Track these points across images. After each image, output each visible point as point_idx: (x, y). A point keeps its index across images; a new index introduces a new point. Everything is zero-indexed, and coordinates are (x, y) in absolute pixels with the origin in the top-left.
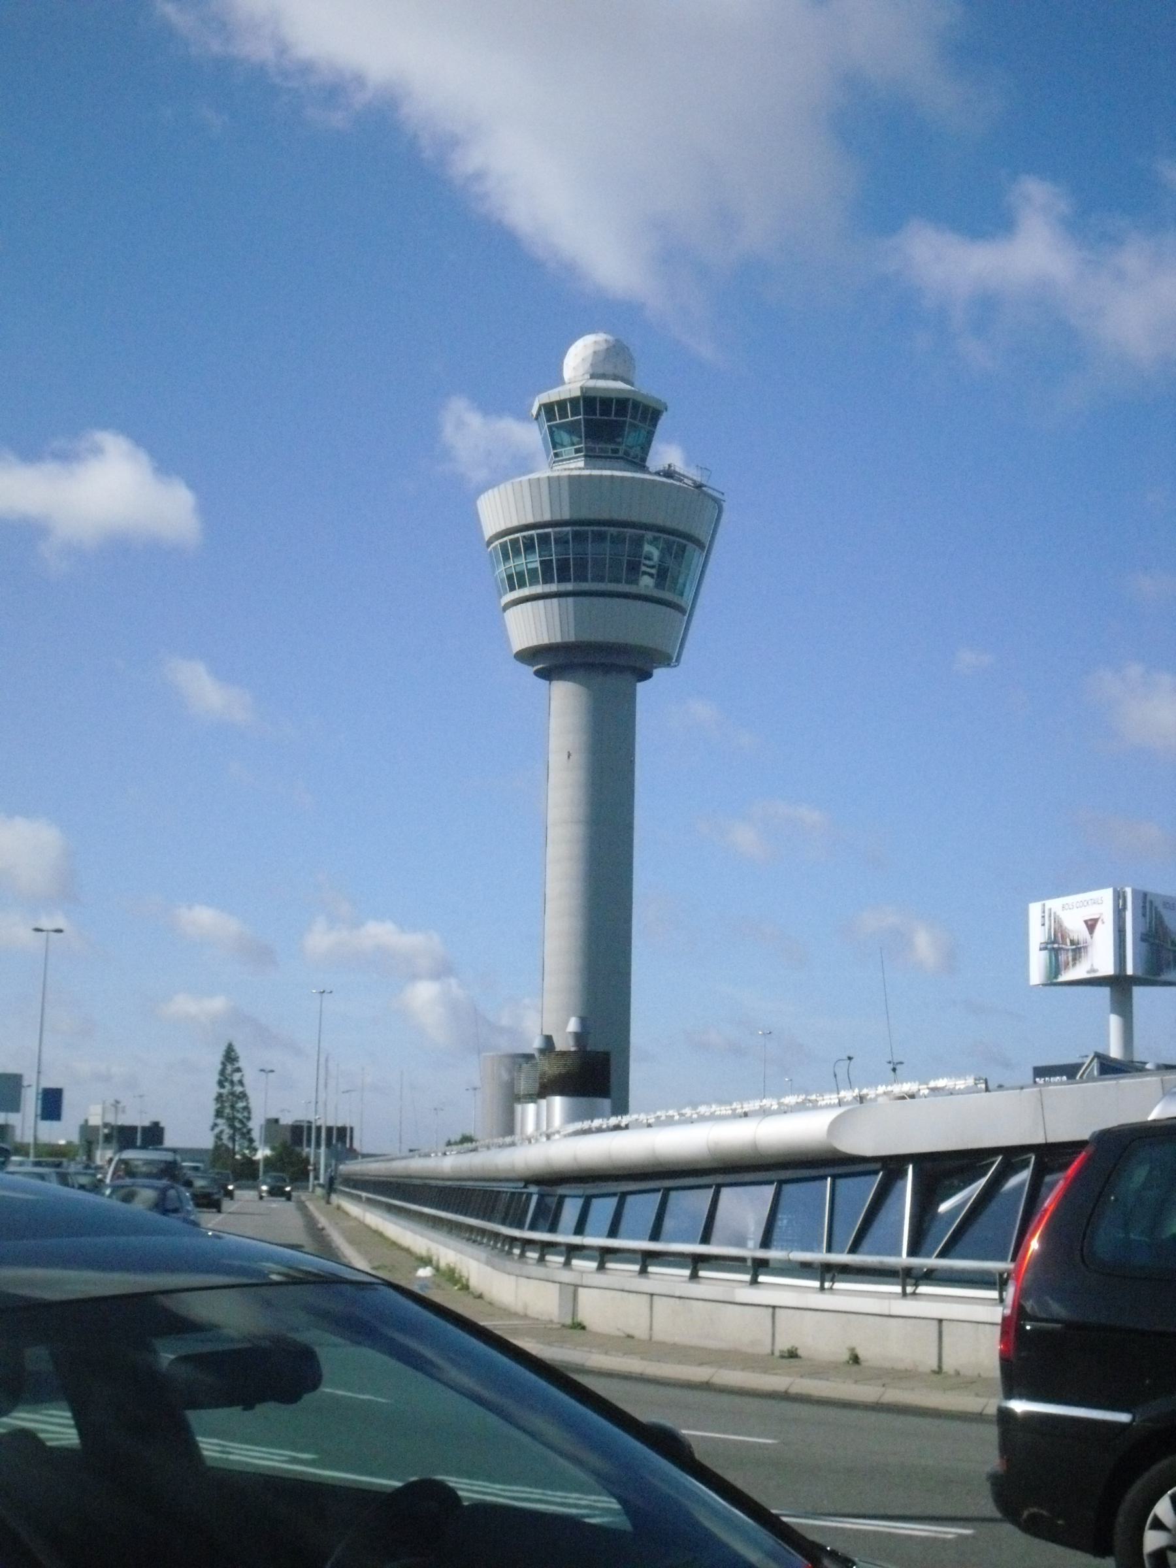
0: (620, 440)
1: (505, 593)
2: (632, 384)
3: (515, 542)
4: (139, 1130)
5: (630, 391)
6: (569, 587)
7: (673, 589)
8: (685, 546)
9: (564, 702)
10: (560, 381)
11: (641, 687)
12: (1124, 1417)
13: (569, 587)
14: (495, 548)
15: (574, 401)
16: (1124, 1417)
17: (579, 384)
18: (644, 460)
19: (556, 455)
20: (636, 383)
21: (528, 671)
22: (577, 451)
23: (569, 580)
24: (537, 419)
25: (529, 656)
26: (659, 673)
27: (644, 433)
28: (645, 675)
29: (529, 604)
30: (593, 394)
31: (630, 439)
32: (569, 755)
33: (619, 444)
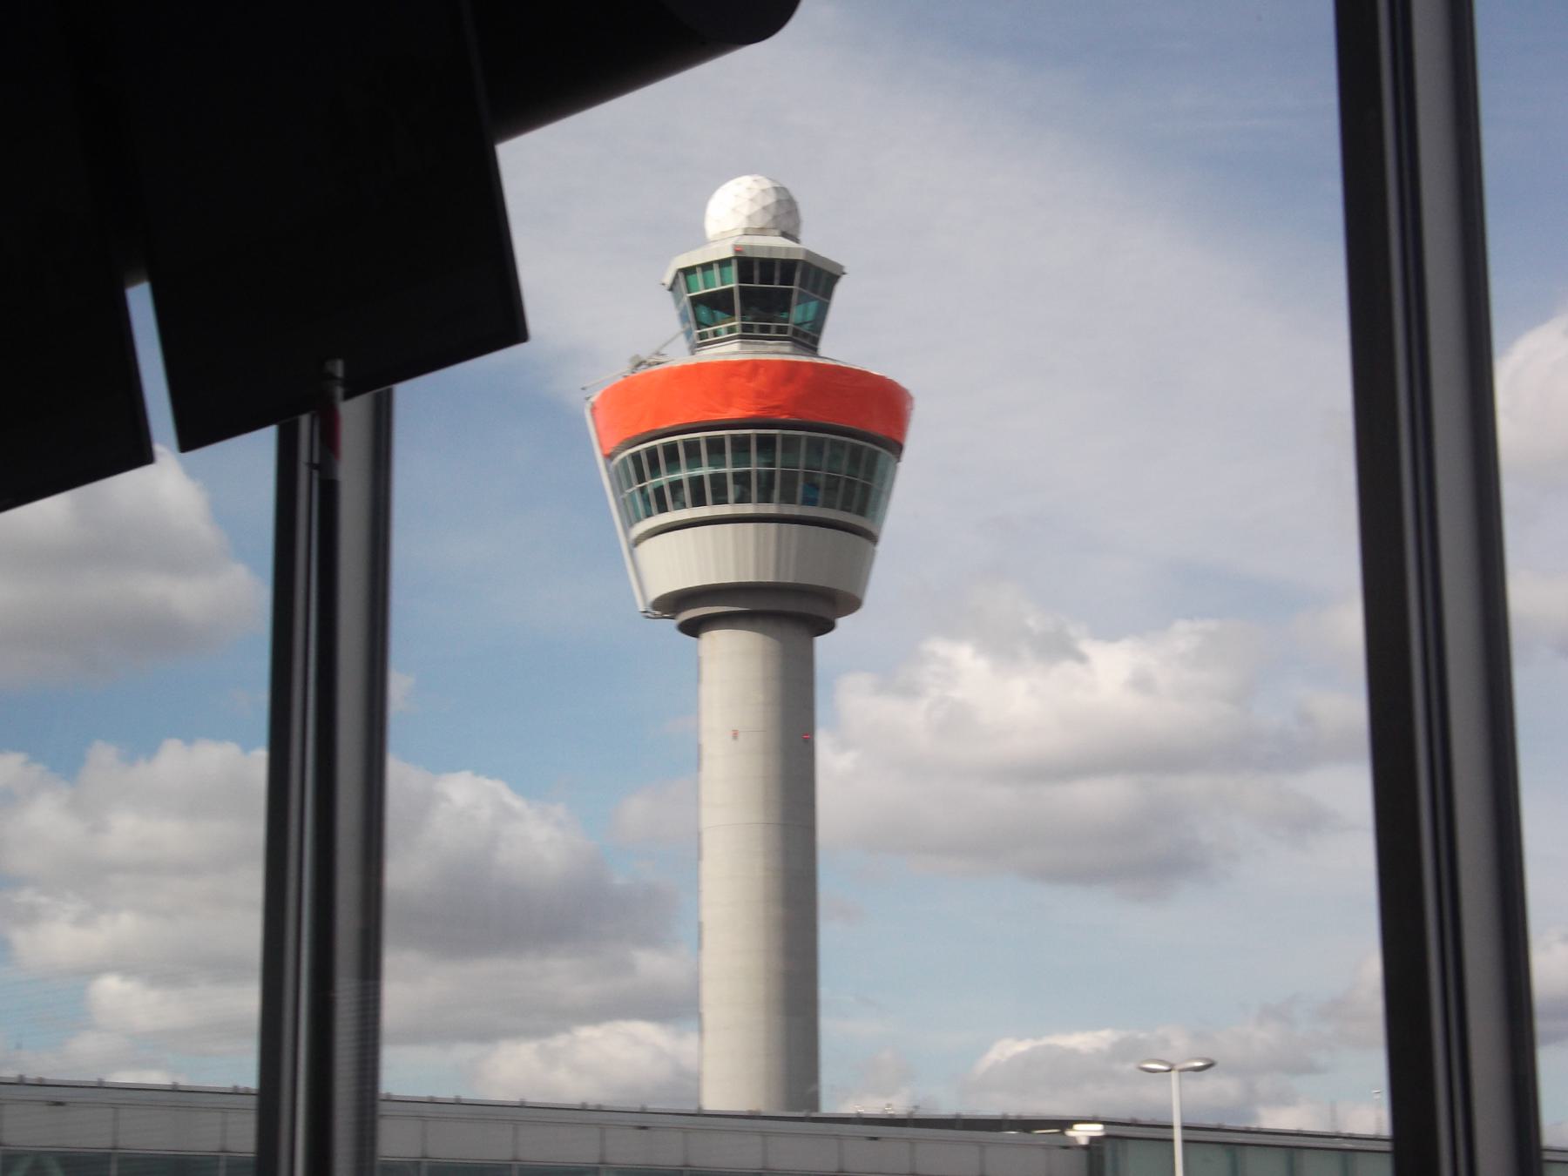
0: (785, 316)
1: (639, 520)
2: (797, 240)
3: (652, 453)
4: (222, 1164)
5: (788, 249)
6: (748, 509)
7: (862, 511)
8: (877, 453)
9: (731, 661)
10: (702, 240)
11: (821, 642)
12: (140, 301)
13: (771, 509)
14: (624, 461)
15: (724, 263)
16: (140, 301)
17: (731, 242)
18: (816, 341)
19: (702, 336)
20: (801, 237)
21: (669, 626)
22: (731, 330)
23: (726, 502)
24: (671, 289)
25: (672, 604)
26: (842, 623)
27: (813, 306)
28: (826, 626)
29: (795, 527)
30: (749, 255)
31: (798, 314)
32: (735, 735)
33: (787, 321)
